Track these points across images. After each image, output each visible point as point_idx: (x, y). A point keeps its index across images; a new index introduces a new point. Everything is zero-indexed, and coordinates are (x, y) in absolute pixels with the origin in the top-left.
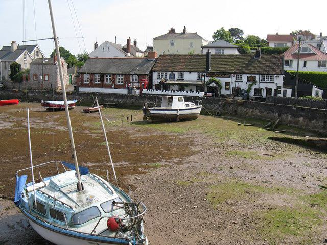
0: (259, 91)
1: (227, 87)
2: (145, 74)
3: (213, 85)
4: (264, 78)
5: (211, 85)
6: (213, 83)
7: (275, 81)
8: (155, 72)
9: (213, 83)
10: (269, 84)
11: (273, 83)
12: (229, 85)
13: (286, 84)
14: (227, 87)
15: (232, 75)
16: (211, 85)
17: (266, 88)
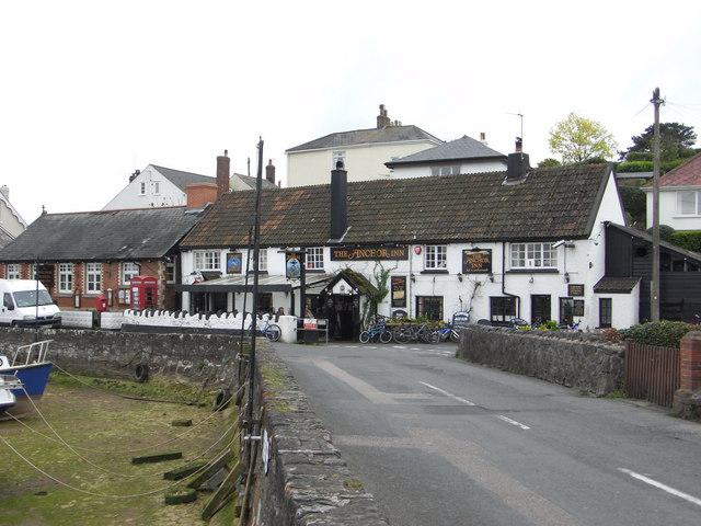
0: (505, 305)
1: (399, 295)
2: (155, 260)
3: (342, 288)
4: (522, 256)
5: (336, 290)
6: (342, 282)
7: (560, 267)
8: (187, 249)
9: (342, 282)
10: (537, 278)
11: (555, 272)
12: (405, 289)
13: (616, 275)
14: (399, 295)
15: (413, 249)
16: (336, 290)
17: (597, 291)
